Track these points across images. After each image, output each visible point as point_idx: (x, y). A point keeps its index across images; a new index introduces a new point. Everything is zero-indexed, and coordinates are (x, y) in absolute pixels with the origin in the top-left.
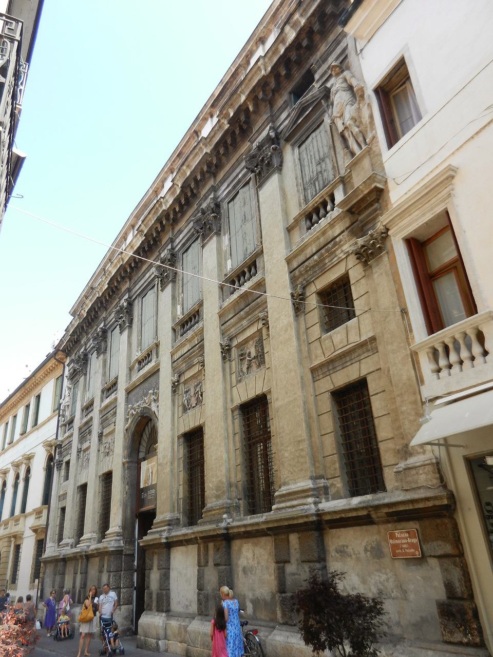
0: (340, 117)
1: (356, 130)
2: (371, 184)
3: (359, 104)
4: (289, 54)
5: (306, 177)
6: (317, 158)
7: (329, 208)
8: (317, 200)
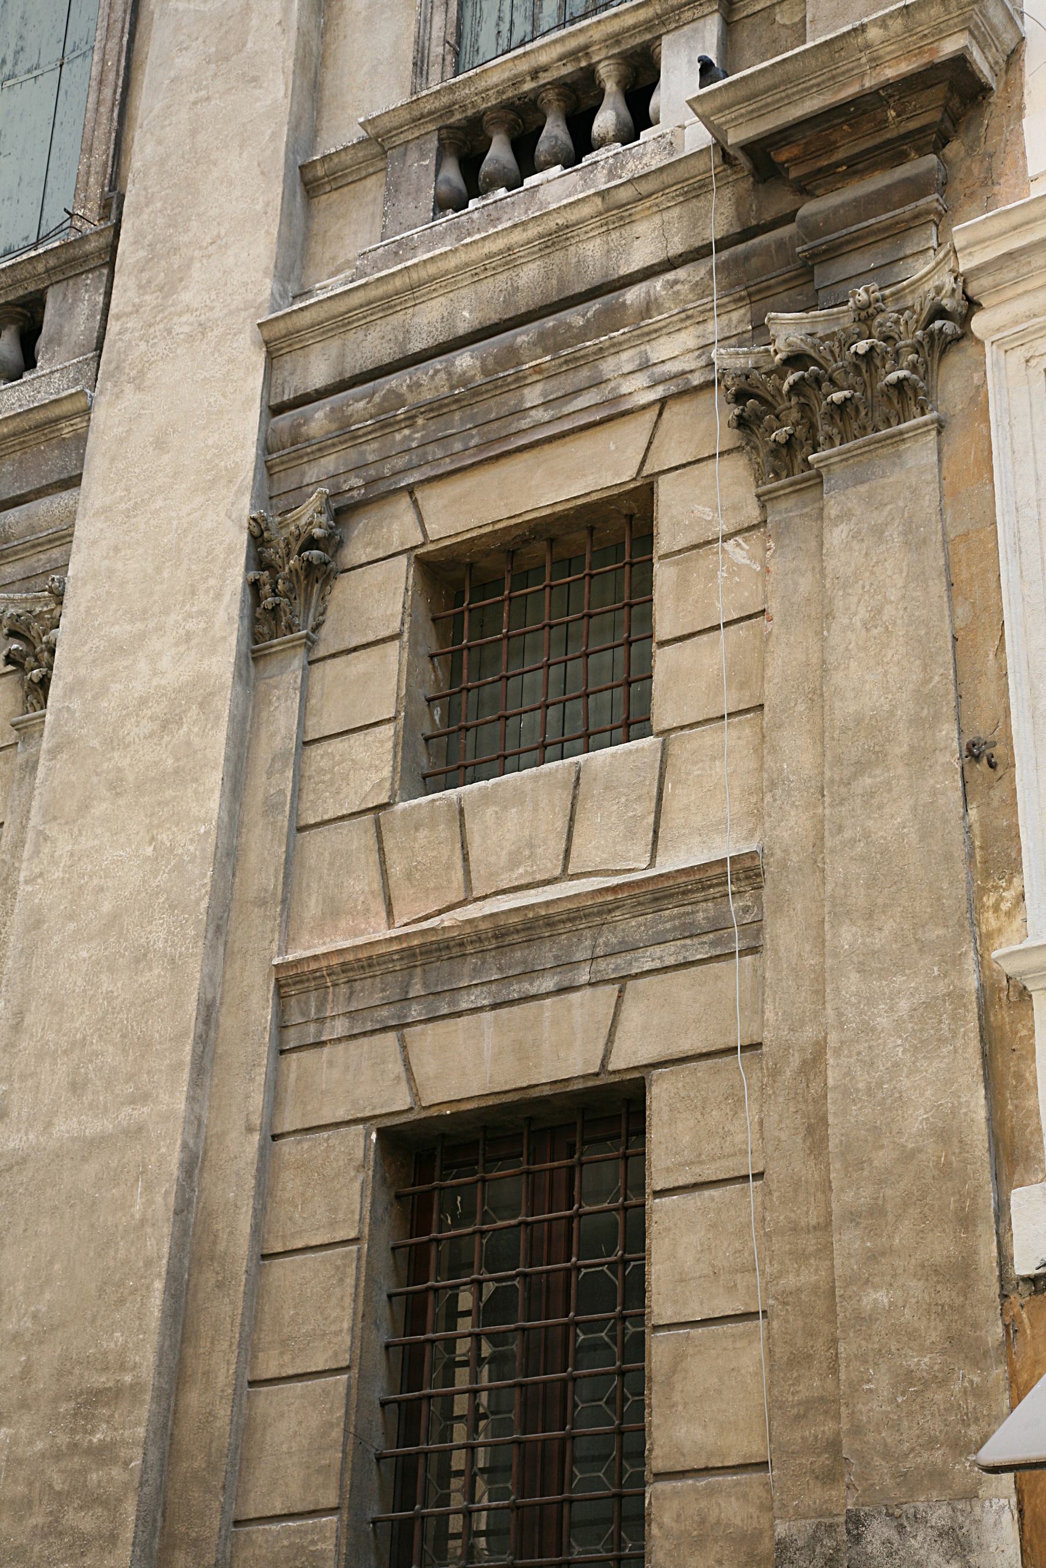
2: (941, 33)
7: (605, 121)
8: (543, 59)
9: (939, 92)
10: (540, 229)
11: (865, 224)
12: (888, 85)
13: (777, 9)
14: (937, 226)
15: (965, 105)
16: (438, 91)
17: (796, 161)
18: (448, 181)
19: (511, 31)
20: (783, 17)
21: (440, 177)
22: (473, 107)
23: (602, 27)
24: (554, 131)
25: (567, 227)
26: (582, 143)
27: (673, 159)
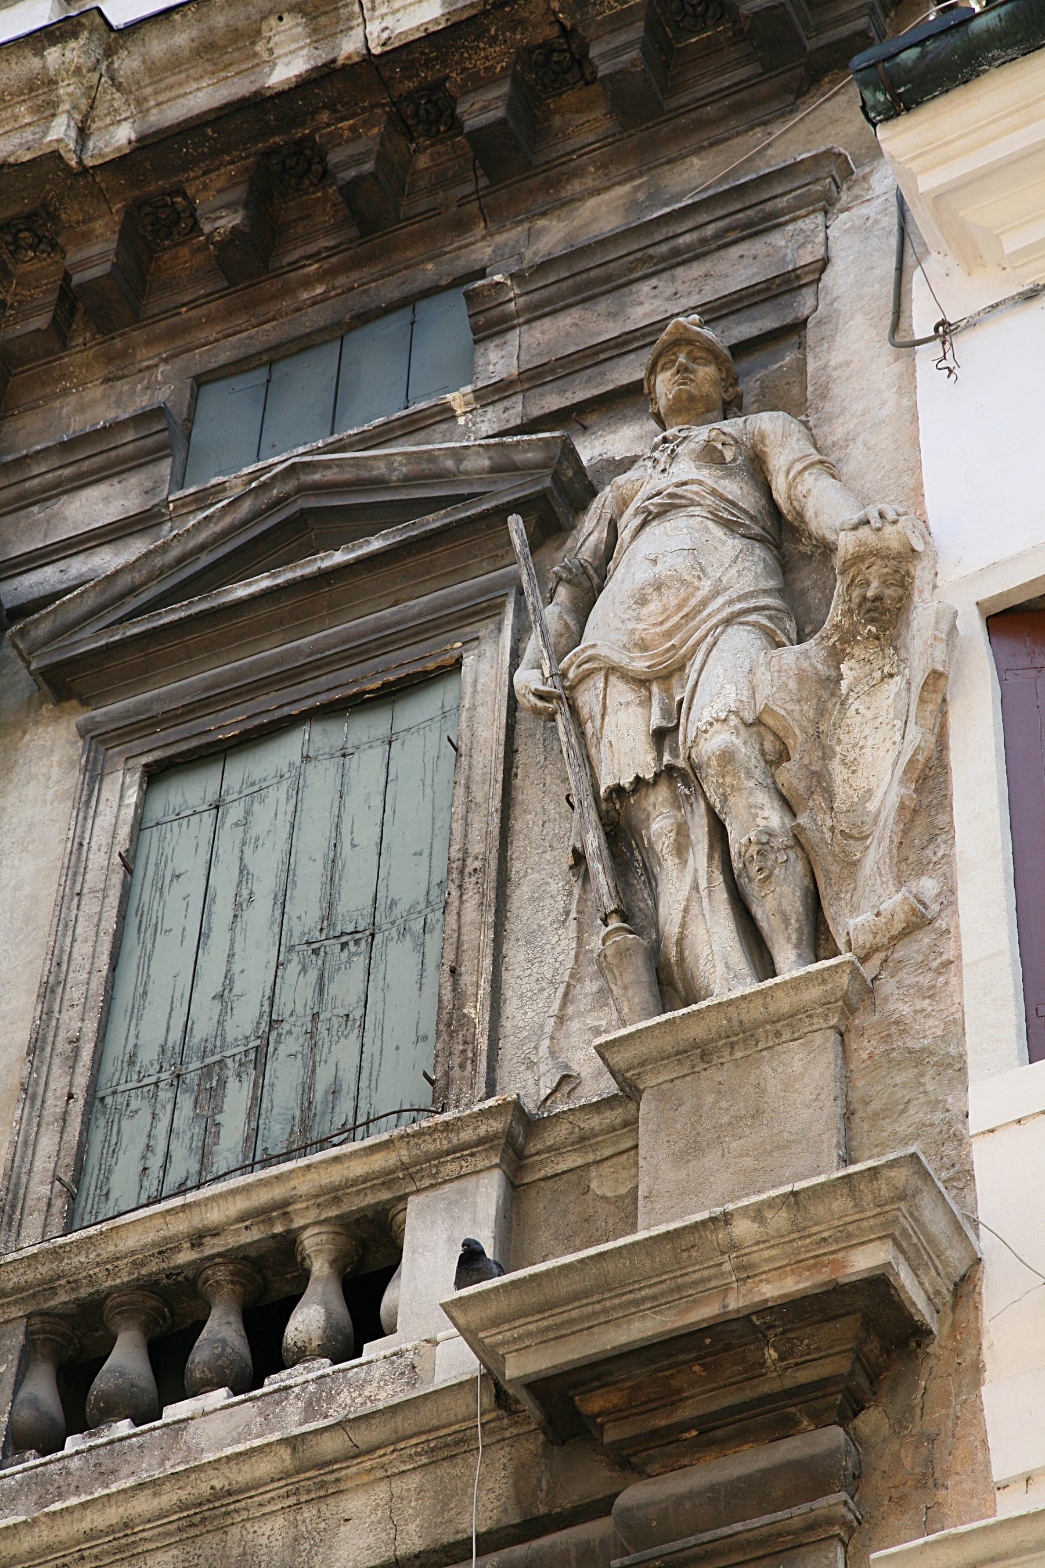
0: (642, 682)
1: (755, 816)
2: (848, 1238)
3: (836, 656)
4: (325, 116)
5: (136, 1014)
6: (305, 912)
7: (307, 1321)
8: (214, 1216)
9: (847, 1328)
10: (182, 1494)
11: (726, 1531)
12: (765, 1310)
13: (593, 1172)
14: (845, 1546)
15: (889, 1352)
16: (34, 1256)
17: (616, 1414)
18: (34, 1403)
19: (164, 1168)
20: (604, 1184)
21: (22, 1395)
22: (91, 1283)
23: (313, 1176)
24: (222, 1332)
25: (230, 1493)
26: (267, 1352)
27: (415, 1394)
